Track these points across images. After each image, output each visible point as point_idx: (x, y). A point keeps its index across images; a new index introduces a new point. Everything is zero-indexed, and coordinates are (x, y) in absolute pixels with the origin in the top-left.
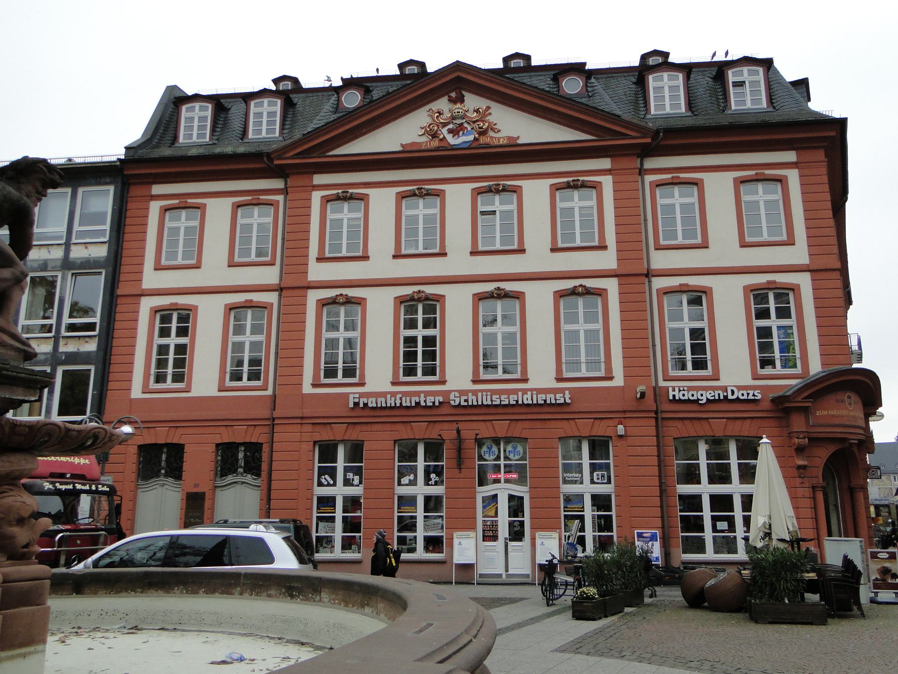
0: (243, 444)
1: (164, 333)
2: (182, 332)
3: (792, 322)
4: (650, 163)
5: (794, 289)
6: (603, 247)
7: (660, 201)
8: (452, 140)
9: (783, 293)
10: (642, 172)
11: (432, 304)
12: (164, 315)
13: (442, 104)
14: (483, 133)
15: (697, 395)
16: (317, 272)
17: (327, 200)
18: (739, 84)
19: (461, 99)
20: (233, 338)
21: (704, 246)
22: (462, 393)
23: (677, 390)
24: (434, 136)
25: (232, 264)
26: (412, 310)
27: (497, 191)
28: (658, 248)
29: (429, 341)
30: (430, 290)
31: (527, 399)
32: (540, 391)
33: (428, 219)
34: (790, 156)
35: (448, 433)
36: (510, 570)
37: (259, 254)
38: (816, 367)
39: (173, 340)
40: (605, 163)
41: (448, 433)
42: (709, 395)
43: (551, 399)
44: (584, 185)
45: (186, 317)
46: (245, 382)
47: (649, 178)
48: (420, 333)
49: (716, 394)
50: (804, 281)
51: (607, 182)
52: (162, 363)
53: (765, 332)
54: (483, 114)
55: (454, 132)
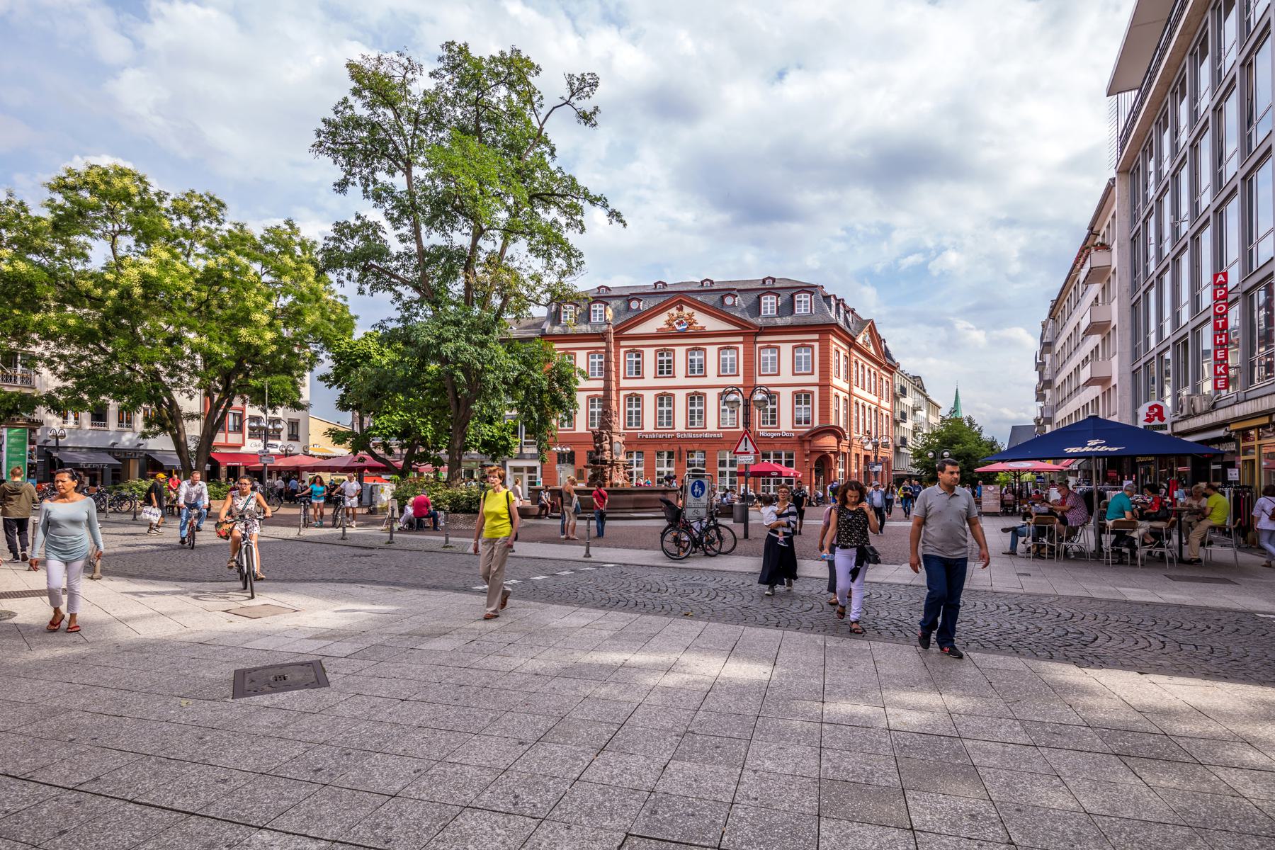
0: (1190, 455)
1: (630, 406)
2: (669, 405)
3: (628, 409)
4: (759, 339)
5: (812, 393)
6: (812, 374)
7: (762, 355)
8: (678, 328)
9: (808, 395)
10: (756, 342)
11: (702, 397)
12: (629, 398)
13: (674, 311)
14: (690, 324)
15: (770, 435)
16: (623, 383)
17: (626, 352)
18: (595, 311)
19: (681, 309)
20: (590, 410)
21: (778, 374)
22: (681, 433)
23: (763, 433)
24: (670, 325)
25: (719, 376)
26: (662, 399)
27: (696, 349)
28: (760, 375)
29: (637, 413)
30: (771, 389)
31: (706, 436)
32: (711, 433)
33: (732, 359)
34: (816, 337)
35: (676, 448)
36: (984, 503)
37: (731, 371)
38: (816, 424)
39: (634, 409)
40: (741, 339)
41: (676, 448)
42: (775, 435)
43: (715, 435)
44: (731, 348)
45: (639, 399)
46: (634, 427)
47: (758, 345)
48: (665, 408)
49: (778, 434)
50: (816, 390)
51: (741, 347)
52: (630, 418)
53: (692, 412)
54: (691, 316)
55: (679, 324)
